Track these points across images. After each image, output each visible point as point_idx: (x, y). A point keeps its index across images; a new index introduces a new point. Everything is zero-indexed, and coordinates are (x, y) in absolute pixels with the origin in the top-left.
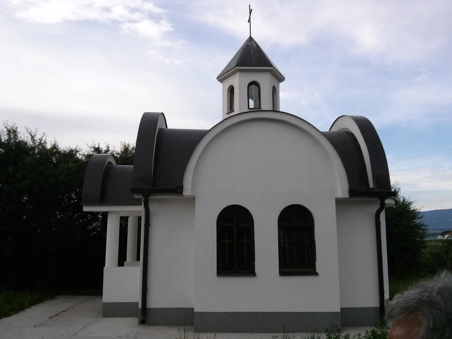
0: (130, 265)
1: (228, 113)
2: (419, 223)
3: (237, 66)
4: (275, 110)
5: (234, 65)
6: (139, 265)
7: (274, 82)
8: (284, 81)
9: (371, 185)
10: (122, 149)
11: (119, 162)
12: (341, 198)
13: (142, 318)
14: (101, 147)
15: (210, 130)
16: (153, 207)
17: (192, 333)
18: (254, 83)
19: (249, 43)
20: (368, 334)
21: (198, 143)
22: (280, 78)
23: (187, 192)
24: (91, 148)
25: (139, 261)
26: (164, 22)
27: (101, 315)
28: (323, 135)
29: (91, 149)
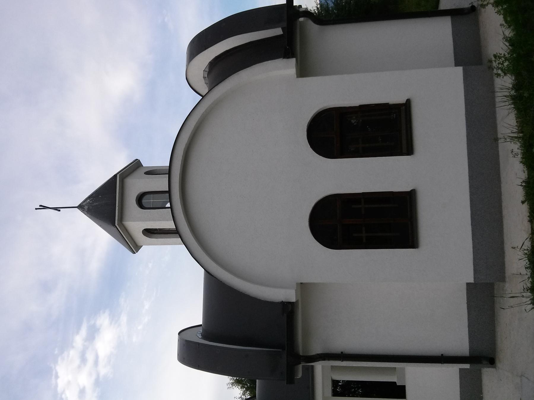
2: (334, 3)
3: (113, 224)
4: (169, 171)
7: (140, 172)
8: (139, 160)
9: (278, 31)
12: (296, 68)
16: (316, 349)
17: (507, 285)
18: (140, 200)
19: (85, 209)
26: (98, 322)
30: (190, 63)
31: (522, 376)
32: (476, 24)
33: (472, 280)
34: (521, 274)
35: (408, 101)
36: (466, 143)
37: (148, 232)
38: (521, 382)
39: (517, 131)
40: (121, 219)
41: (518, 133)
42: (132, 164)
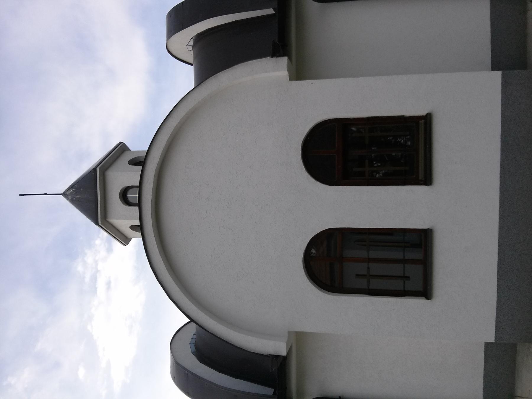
9: (270, 11)
33: (492, 339)
36: (500, 169)
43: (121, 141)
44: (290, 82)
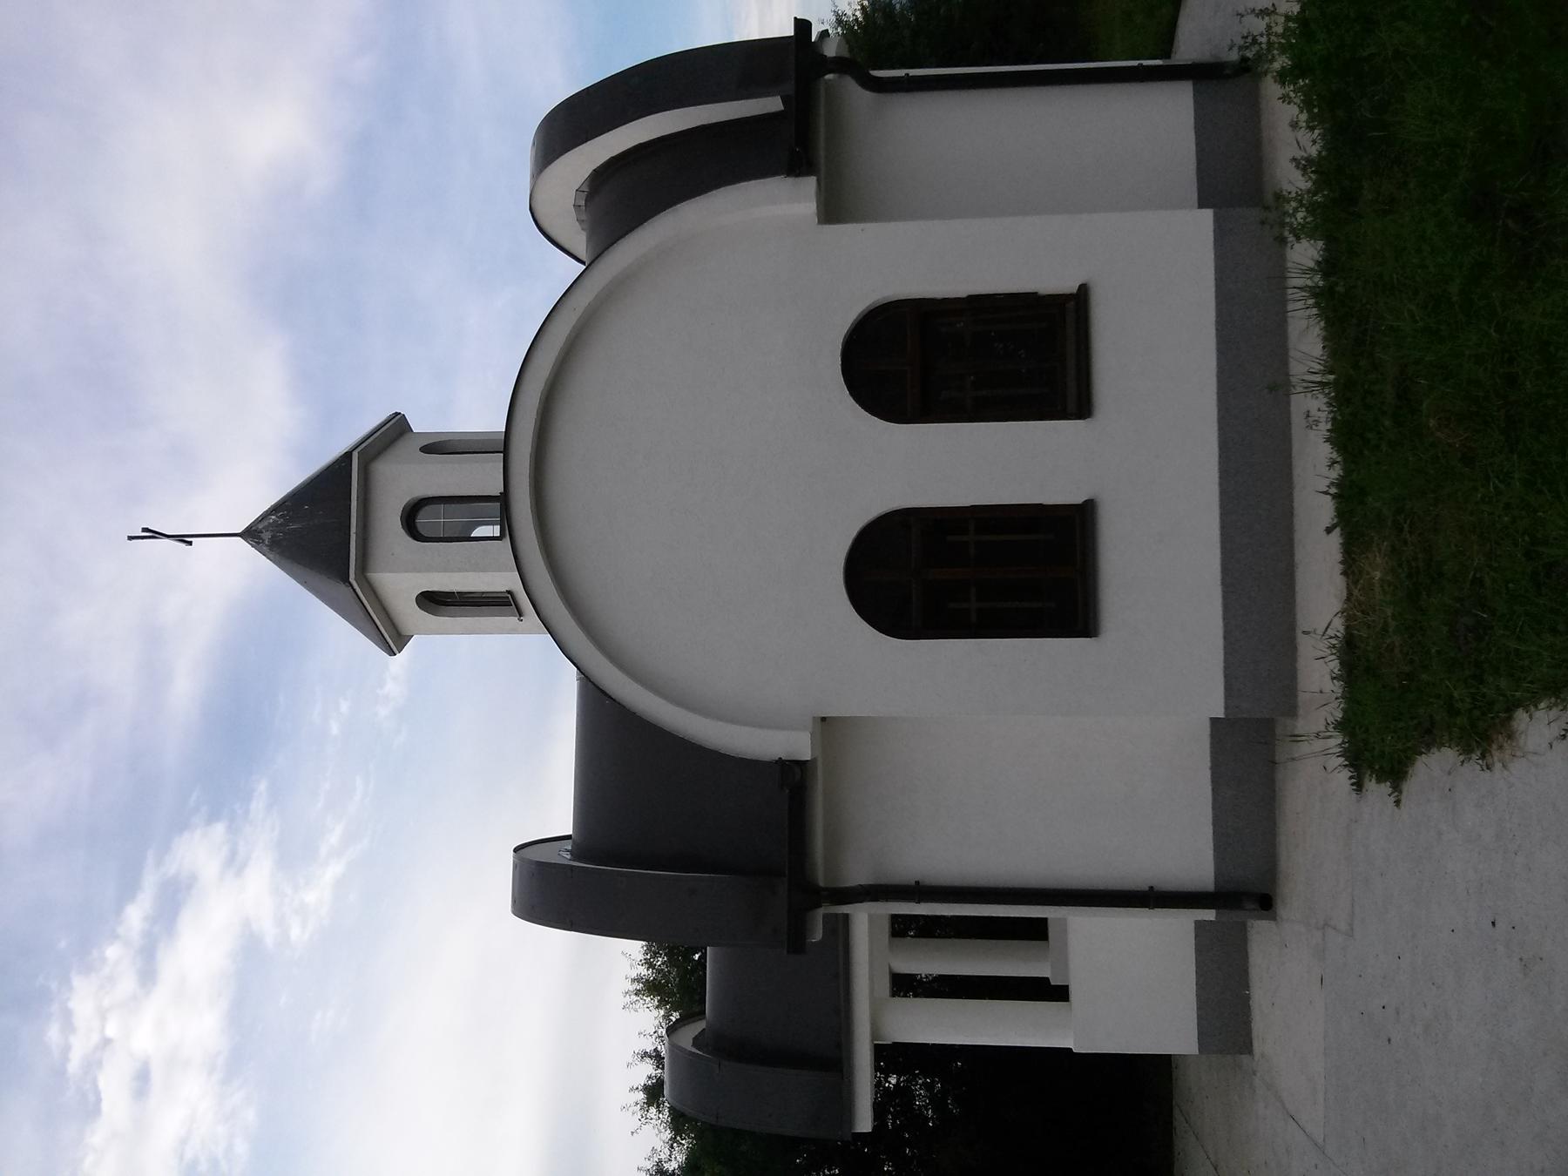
0: (1063, 962)
1: (521, 614)
3: (345, 579)
4: (503, 446)
5: (343, 588)
6: (1063, 923)
9: (773, 104)
10: (650, 1005)
11: (696, 1009)
12: (817, 203)
13: (1253, 906)
14: (642, 1080)
15: (577, 667)
16: (857, 874)
18: (410, 518)
20: (1292, 95)
21: (624, 707)
22: (396, 428)
23: (798, 745)
24: (647, 1118)
25: (1046, 919)
27: (1245, 1058)
28: (597, 261)
29: (653, 1116)
30: (547, 169)
31: (1326, 924)
32: (1253, 108)
33: (1220, 713)
34: (1321, 692)
35: (1084, 290)
37: (431, 601)
38: (1324, 940)
39: (1322, 368)
40: (363, 567)
41: (1324, 373)
42: (388, 425)
43: (399, 411)
44: (820, 226)
